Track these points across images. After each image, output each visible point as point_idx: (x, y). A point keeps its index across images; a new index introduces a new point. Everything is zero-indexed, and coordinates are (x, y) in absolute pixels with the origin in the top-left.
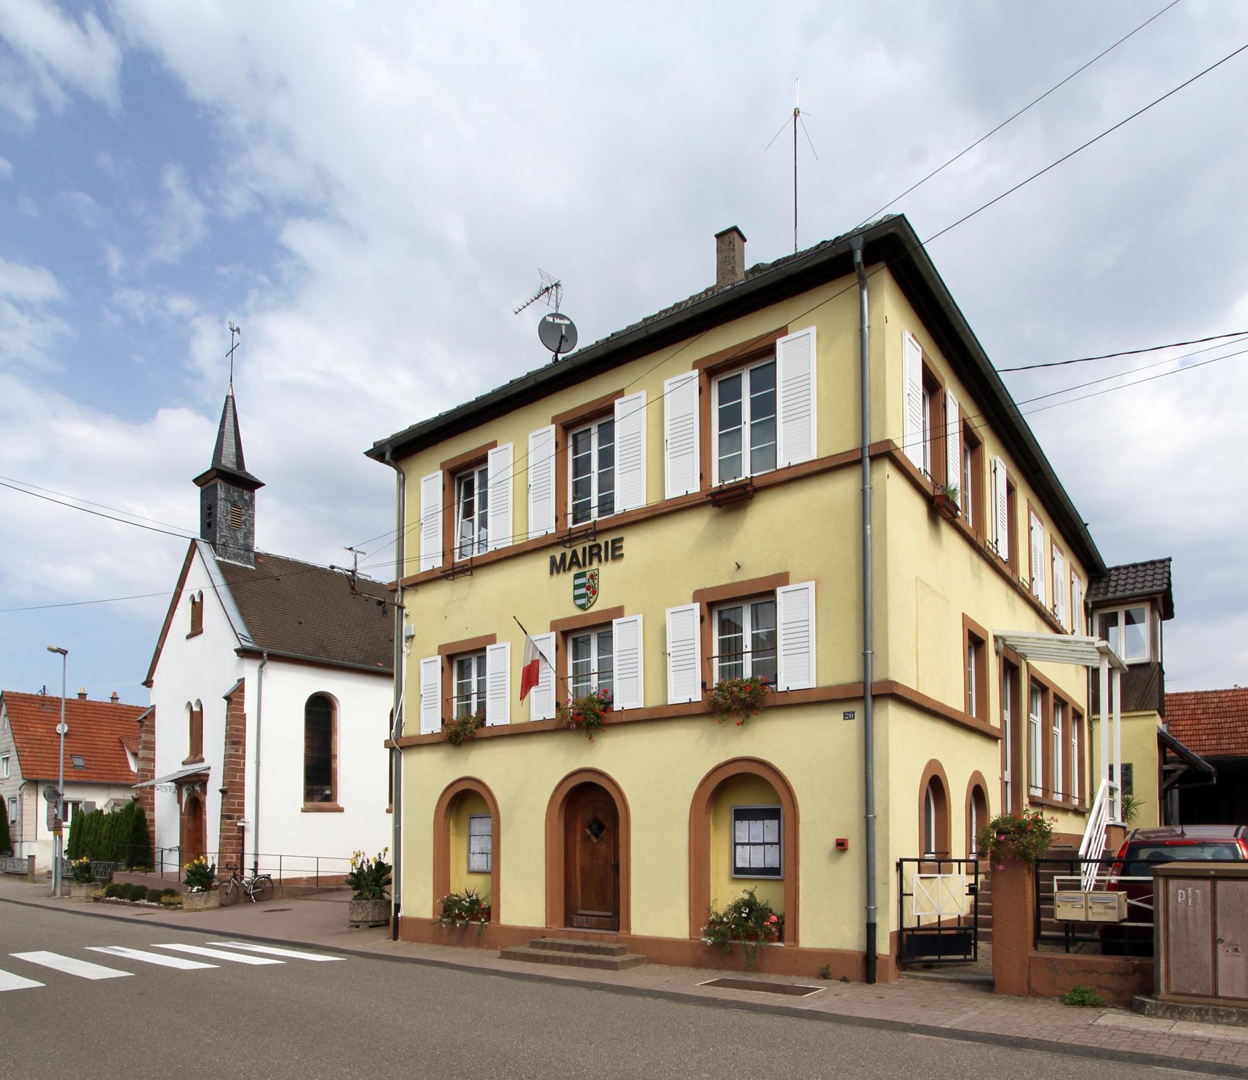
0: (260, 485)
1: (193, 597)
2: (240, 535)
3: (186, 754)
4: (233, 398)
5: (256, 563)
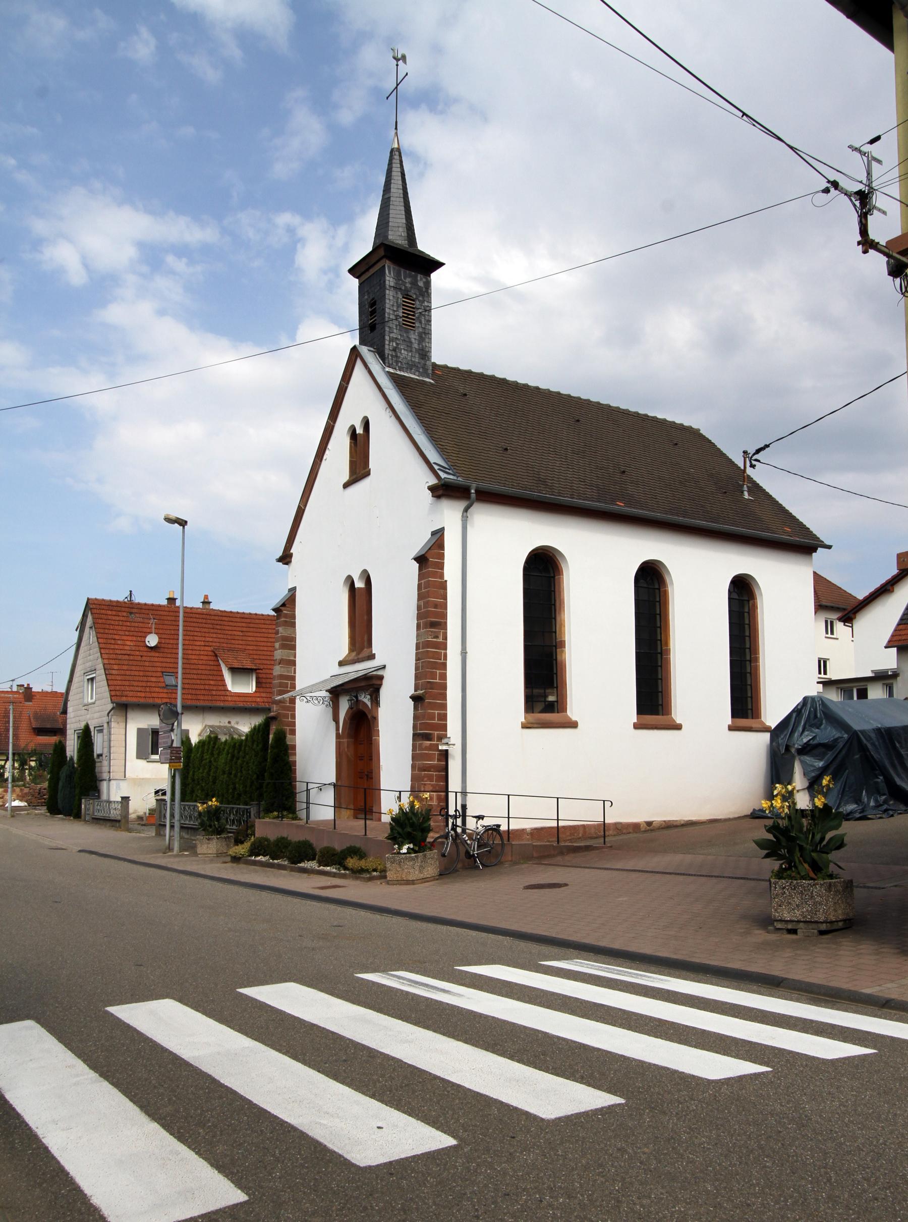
0: (438, 265)
1: (353, 430)
2: (413, 336)
3: (343, 649)
4: (399, 150)
5: (434, 376)
